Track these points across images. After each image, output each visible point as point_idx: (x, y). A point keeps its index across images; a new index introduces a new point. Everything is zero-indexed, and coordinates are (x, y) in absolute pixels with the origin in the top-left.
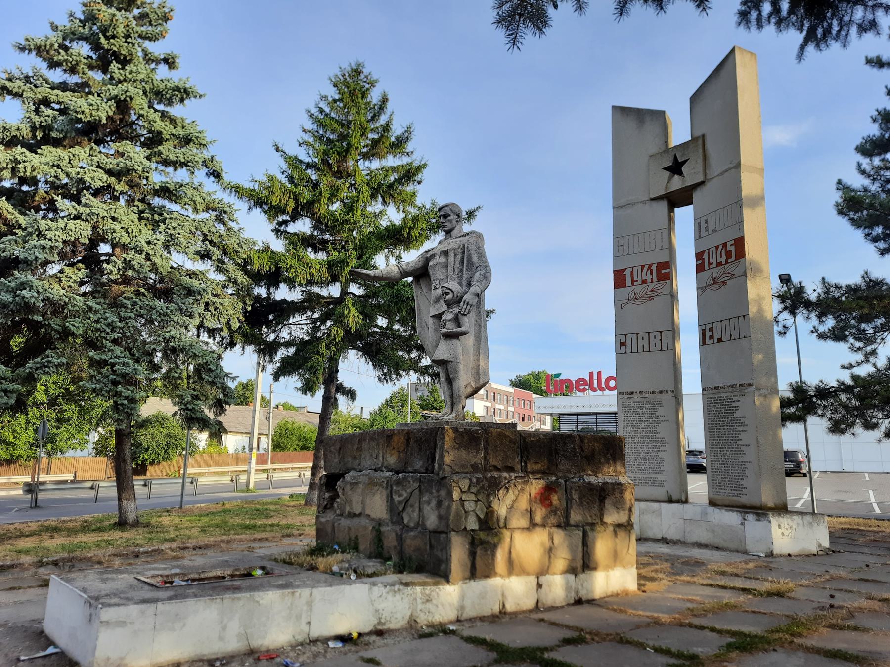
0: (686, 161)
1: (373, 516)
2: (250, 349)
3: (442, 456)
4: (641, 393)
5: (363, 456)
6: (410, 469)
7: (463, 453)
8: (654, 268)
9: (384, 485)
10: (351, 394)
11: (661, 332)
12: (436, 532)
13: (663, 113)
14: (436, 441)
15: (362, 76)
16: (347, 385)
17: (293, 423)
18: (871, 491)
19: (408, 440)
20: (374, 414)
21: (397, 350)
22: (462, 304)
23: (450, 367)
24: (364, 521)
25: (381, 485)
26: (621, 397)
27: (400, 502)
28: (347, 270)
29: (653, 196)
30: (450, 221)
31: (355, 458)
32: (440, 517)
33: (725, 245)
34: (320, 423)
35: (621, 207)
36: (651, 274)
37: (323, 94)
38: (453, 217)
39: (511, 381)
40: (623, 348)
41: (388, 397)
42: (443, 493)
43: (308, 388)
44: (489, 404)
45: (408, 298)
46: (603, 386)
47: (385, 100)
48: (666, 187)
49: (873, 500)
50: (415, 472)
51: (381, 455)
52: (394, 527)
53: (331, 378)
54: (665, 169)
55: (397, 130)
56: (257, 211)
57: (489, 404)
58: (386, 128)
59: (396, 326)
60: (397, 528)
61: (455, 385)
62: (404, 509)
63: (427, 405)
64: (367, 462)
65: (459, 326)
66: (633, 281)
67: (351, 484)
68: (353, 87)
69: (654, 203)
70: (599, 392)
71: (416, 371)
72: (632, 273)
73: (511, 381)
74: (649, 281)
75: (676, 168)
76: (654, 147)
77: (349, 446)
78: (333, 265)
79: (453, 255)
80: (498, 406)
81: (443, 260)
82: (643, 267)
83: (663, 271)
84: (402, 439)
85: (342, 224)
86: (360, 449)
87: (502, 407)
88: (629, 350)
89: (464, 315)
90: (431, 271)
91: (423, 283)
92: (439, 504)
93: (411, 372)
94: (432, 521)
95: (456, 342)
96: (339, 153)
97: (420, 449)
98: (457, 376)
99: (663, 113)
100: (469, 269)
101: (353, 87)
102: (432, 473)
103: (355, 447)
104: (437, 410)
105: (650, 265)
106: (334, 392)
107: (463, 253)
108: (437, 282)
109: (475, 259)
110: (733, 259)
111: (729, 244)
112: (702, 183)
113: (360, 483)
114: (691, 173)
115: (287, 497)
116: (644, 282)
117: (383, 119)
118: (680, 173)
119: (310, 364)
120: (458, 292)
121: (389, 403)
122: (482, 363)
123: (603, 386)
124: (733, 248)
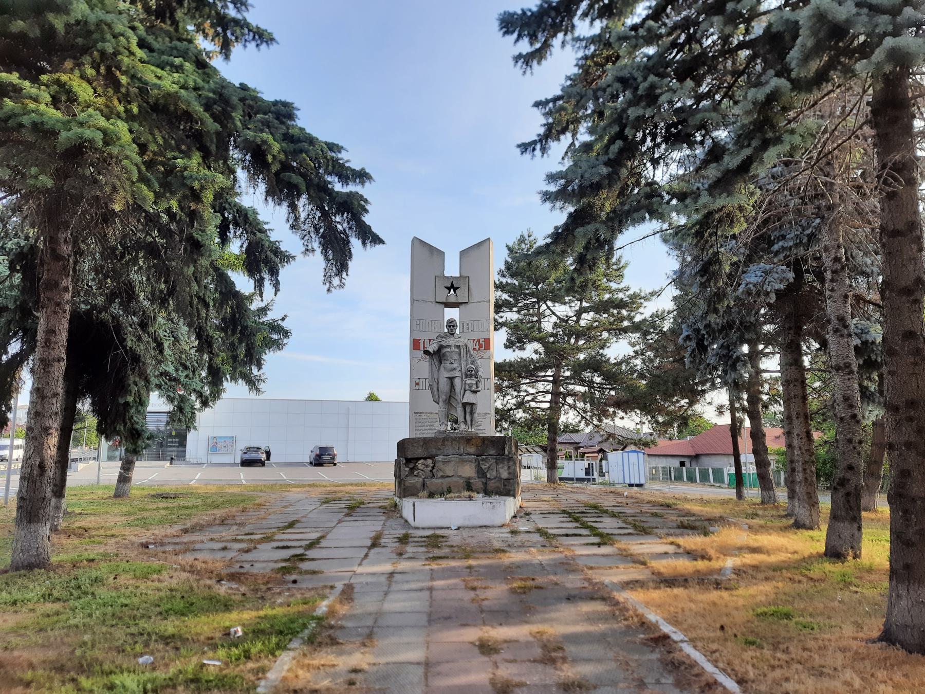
24: (454, 479)
32: (509, 473)
42: (511, 463)
60: (483, 480)
92: (509, 468)
94: (505, 475)
114: (462, 296)
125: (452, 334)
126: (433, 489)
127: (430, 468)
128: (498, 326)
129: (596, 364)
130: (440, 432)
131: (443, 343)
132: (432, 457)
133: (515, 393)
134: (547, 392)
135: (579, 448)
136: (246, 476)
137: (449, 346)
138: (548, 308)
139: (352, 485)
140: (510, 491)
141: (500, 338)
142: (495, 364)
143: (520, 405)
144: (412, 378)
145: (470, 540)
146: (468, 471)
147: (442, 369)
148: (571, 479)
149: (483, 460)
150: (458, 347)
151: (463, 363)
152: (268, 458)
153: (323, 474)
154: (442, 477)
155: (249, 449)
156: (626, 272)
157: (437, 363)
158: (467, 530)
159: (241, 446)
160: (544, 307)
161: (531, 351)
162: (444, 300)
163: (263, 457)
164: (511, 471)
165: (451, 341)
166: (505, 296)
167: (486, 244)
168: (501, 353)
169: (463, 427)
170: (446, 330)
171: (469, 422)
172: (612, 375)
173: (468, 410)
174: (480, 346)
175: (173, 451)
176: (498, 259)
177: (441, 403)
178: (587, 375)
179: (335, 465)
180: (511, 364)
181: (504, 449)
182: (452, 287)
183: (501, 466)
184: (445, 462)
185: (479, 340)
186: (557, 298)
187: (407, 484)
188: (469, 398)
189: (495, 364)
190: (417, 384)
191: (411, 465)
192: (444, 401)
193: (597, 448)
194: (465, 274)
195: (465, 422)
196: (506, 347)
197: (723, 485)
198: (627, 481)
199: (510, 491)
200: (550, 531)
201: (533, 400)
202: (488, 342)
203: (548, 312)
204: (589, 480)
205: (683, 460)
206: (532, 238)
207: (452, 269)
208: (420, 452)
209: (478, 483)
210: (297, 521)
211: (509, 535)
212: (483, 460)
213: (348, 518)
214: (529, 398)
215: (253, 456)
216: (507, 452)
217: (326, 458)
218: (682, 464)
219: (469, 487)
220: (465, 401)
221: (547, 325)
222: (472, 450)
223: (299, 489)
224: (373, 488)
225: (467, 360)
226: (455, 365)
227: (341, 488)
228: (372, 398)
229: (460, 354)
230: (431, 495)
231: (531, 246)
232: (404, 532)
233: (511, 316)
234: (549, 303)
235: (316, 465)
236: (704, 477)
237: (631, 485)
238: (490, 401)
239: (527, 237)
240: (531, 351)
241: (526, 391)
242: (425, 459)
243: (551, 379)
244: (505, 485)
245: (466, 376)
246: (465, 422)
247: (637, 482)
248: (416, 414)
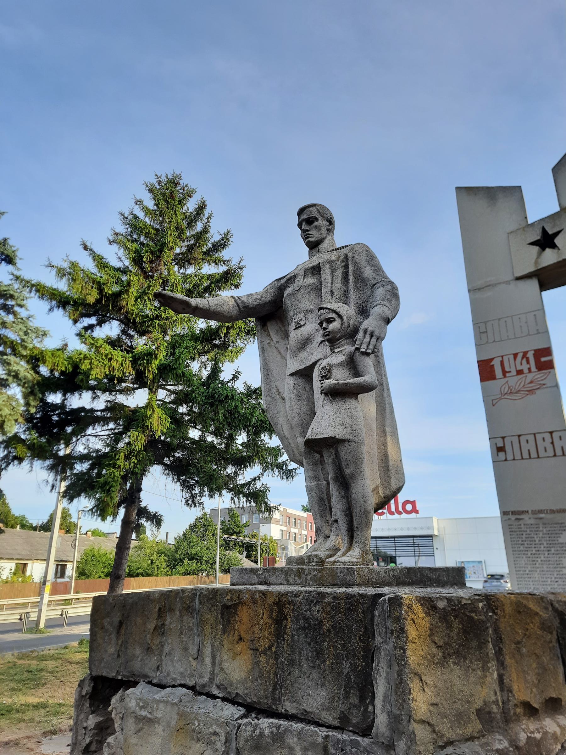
2: (38, 463)
3: (400, 690)
4: (534, 512)
5: (166, 649)
6: (288, 707)
7: (455, 673)
8: (530, 355)
10: (157, 520)
11: (551, 433)
13: (518, 189)
14: (369, 634)
15: (179, 188)
16: (152, 509)
17: (99, 549)
19: (279, 622)
20: (179, 540)
21: (211, 462)
22: (360, 336)
23: (344, 451)
25: (209, 743)
26: (506, 517)
28: (155, 364)
30: (318, 228)
31: (149, 650)
34: (117, 553)
35: (479, 289)
36: (528, 362)
37: (138, 199)
38: (321, 222)
39: (303, 506)
40: (502, 454)
41: (192, 523)
43: (102, 510)
44: (285, 528)
45: (227, 396)
46: (400, 509)
47: (201, 208)
48: (536, 263)
50: (305, 718)
51: (207, 652)
53: (132, 498)
54: (533, 244)
55: (215, 236)
56: (59, 313)
57: (285, 528)
58: (205, 231)
59: (209, 438)
61: (356, 490)
63: (228, 529)
64: (176, 667)
65: (357, 374)
66: (504, 373)
67: (139, 719)
68: (169, 194)
69: (521, 283)
70: (396, 516)
71: (230, 490)
72: (502, 363)
73: (303, 506)
74: (526, 371)
75: (546, 241)
76: (511, 224)
77: (139, 621)
78: (139, 359)
79: (328, 271)
80: (293, 530)
81: (310, 280)
82: (515, 355)
83: (543, 359)
84: (264, 619)
85: (152, 320)
86: (160, 630)
87: (296, 531)
88: (510, 457)
89: (366, 354)
90: (288, 303)
91: (272, 329)
93: (224, 492)
95: (351, 403)
96: (152, 253)
97: (319, 654)
98: (358, 471)
99: (518, 189)
100: (359, 289)
101: (169, 194)
102: (366, 732)
103: (151, 626)
104: (238, 534)
105: (525, 353)
106: (137, 515)
107: (346, 267)
108: (301, 316)
109: (368, 272)
115: (76, 644)
116: (520, 372)
117: (199, 227)
118: (554, 246)
119: (108, 485)
120: (350, 318)
121: (193, 528)
122: (391, 450)
123: (400, 509)
190: (500, 449)
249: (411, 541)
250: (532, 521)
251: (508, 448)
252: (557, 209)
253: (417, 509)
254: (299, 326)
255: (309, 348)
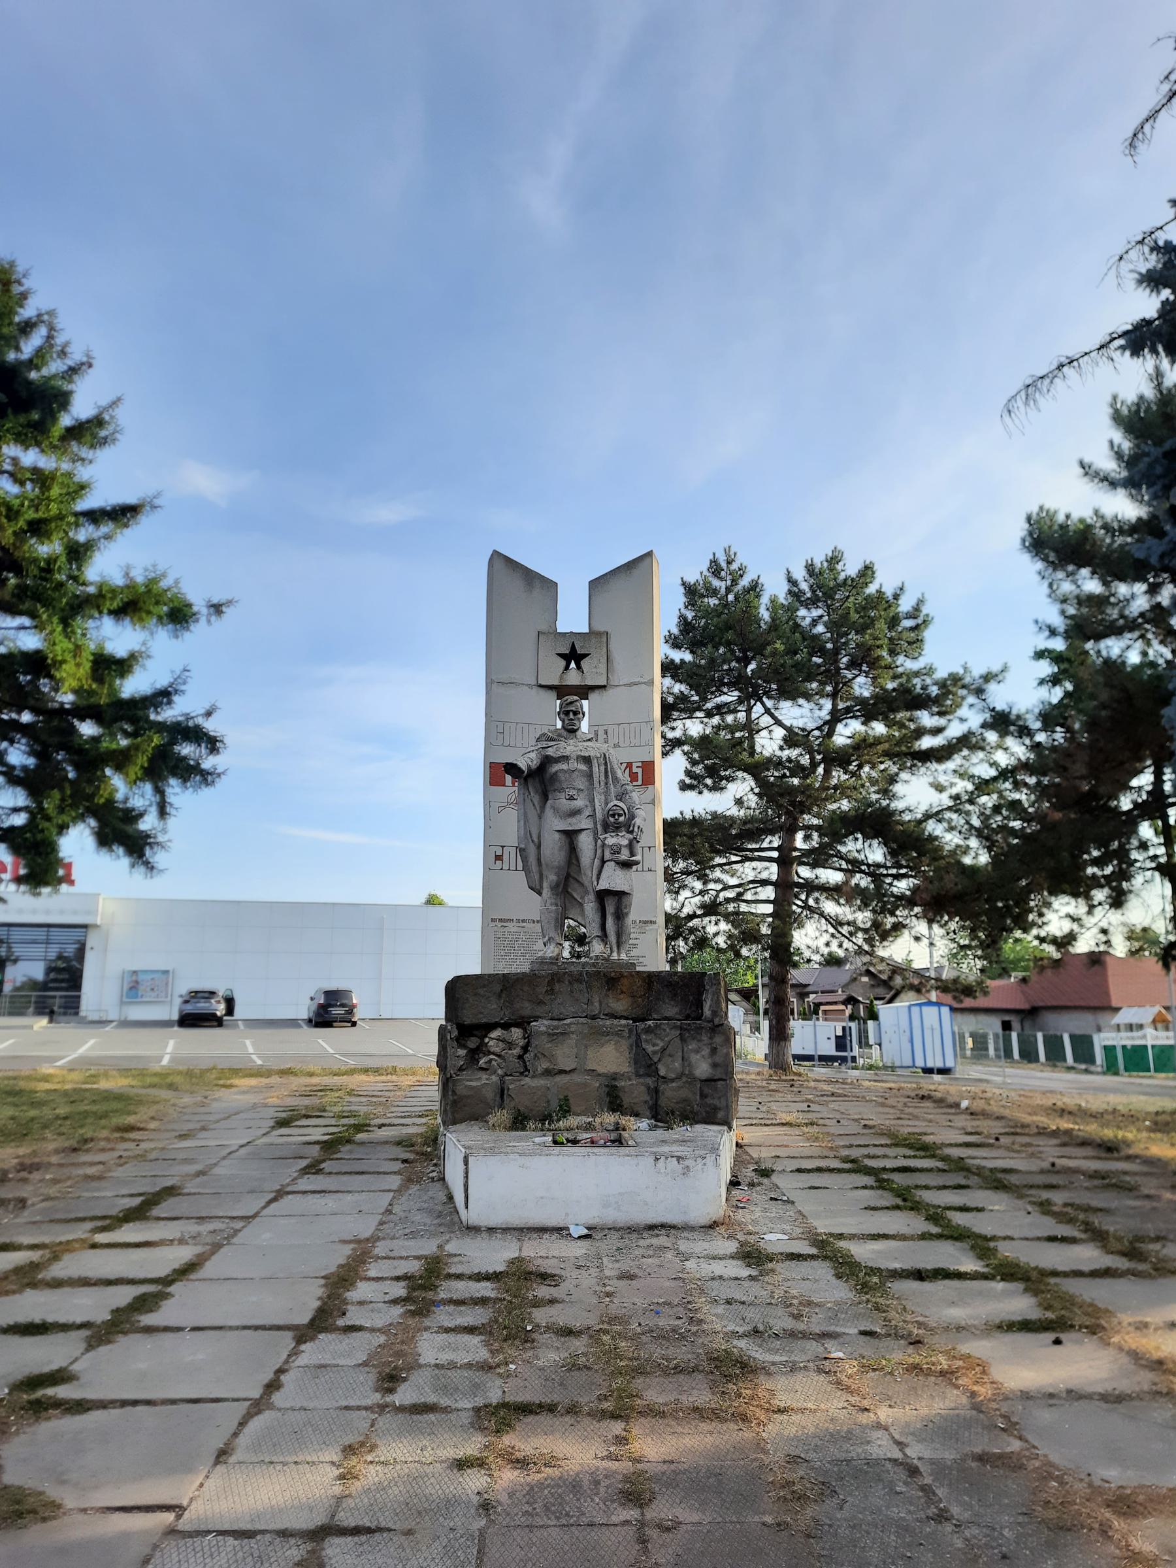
0: (587, 655)
1: (601, 1069)
4: (518, 921)
6: (655, 1016)
9: (626, 1034)
12: (710, 1080)
13: (495, 552)
18: (320, 1041)
23: (625, 900)
24: (577, 1078)
27: (655, 1053)
29: (543, 683)
32: (715, 1065)
33: (629, 765)
42: (718, 1039)
48: (561, 678)
49: (251, 1050)
52: (641, 1080)
54: (559, 655)
60: (650, 1081)
62: (659, 1060)
69: (542, 692)
88: (506, 867)
92: (714, 1051)
94: (703, 1069)
110: (640, 782)
111: (634, 765)
112: (604, 687)
113: (573, 1033)
114: (592, 672)
124: (640, 771)
125: (571, 731)
126: (524, 1103)
127: (517, 1051)
128: (672, 745)
129: (877, 822)
130: (542, 961)
131: (550, 752)
132: (522, 1023)
133: (698, 885)
134: (764, 883)
135: (807, 994)
136: (173, 1048)
137: (565, 758)
138: (768, 711)
139: (366, 1071)
140: (716, 1109)
141: (672, 769)
142: (665, 821)
143: (711, 909)
144: (487, 845)
145: (629, 1298)
146: (611, 1058)
147: (549, 812)
148: (809, 1058)
149: (648, 1030)
150: (587, 760)
151: (599, 800)
152: (230, 1010)
153: (327, 1041)
154: (548, 1073)
155: (195, 995)
156: (928, 634)
157: (536, 799)
158: (614, 1235)
159: (184, 985)
160: (758, 709)
161: (735, 797)
162: (556, 683)
163: (220, 1009)
164: (718, 1059)
165: (570, 747)
166: (679, 688)
167: (648, 560)
168: (673, 798)
169: (597, 948)
170: (559, 725)
171: (612, 938)
172: (907, 841)
173: (610, 909)
174: (634, 777)
175: (642, 1071)
176: (668, 610)
177: (546, 892)
178: (852, 846)
179: (354, 1024)
180: (695, 822)
181: (699, 1004)
182: (573, 656)
183: (693, 1045)
184: (555, 1036)
185: (629, 765)
186: (790, 693)
187: (460, 1090)
188: (613, 878)
189: (665, 821)
190: (499, 858)
191: (473, 1043)
192: (554, 888)
193: (841, 995)
194: (600, 628)
195: (604, 937)
196: (684, 787)
197: (1092, 1068)
198: (920, 1063)
199: (716, 1109)
200: (863, 1252)
201: (739, 898)
202: (648, 769)
203: (766, 720)
204: (843, 1060)
205: (1007, 1018)
206: (735, 566)
207: (573, 616)
208: (489, 1009)
209: (635, 1090)
210: (170, 1191)
211: (740, 1270)
212: (648, 1030)
213: (305, 1183)
214: (731, 894)
215: (202, 1006)
216: (707, 1012)
217: (338, 1011)
218: (1007, 1026)
219: (614, 1102)
220: (603, 885)
221: (769, 744)
222: (620, 1005)
223: (253, 1082)
224: (408, 1080)
225: (607, 793)
226: (580, 803)
227: (337, 1080)
228: (432, 901)
229: (590, 776)
230: (519, 1123)
231: (734, 582)
232: (429, 1247)
233: (695, 727)
234: (769, 703)
235: (319, 1025)
236: (1055, 1054)
237: (928, 1071)
238: (657, 897)
239: (724, 565)
240: (735, 797)
241: (718, 881)
242: (506, 1026)
243: (775, 854)
244: (703, 1096)
245: (606, 827)
246: (604, 937)
247: (939, 1064)
248: (495, 922)
249: (41, 934)
250: (515, 929)
251: (506, 857)
252: (587, 631)
253: (73, 878)
254: (572, 798)
255: (578, 817)
